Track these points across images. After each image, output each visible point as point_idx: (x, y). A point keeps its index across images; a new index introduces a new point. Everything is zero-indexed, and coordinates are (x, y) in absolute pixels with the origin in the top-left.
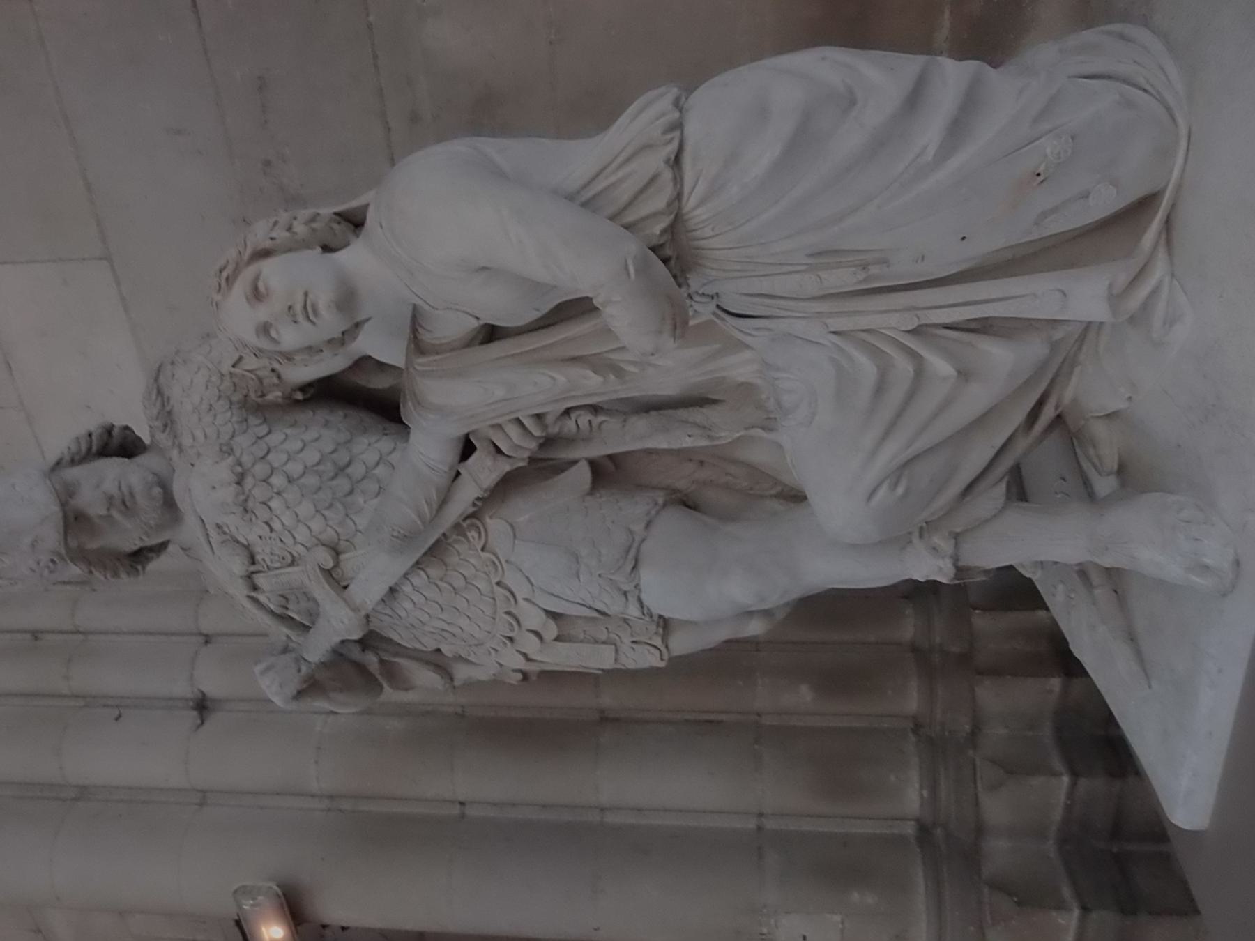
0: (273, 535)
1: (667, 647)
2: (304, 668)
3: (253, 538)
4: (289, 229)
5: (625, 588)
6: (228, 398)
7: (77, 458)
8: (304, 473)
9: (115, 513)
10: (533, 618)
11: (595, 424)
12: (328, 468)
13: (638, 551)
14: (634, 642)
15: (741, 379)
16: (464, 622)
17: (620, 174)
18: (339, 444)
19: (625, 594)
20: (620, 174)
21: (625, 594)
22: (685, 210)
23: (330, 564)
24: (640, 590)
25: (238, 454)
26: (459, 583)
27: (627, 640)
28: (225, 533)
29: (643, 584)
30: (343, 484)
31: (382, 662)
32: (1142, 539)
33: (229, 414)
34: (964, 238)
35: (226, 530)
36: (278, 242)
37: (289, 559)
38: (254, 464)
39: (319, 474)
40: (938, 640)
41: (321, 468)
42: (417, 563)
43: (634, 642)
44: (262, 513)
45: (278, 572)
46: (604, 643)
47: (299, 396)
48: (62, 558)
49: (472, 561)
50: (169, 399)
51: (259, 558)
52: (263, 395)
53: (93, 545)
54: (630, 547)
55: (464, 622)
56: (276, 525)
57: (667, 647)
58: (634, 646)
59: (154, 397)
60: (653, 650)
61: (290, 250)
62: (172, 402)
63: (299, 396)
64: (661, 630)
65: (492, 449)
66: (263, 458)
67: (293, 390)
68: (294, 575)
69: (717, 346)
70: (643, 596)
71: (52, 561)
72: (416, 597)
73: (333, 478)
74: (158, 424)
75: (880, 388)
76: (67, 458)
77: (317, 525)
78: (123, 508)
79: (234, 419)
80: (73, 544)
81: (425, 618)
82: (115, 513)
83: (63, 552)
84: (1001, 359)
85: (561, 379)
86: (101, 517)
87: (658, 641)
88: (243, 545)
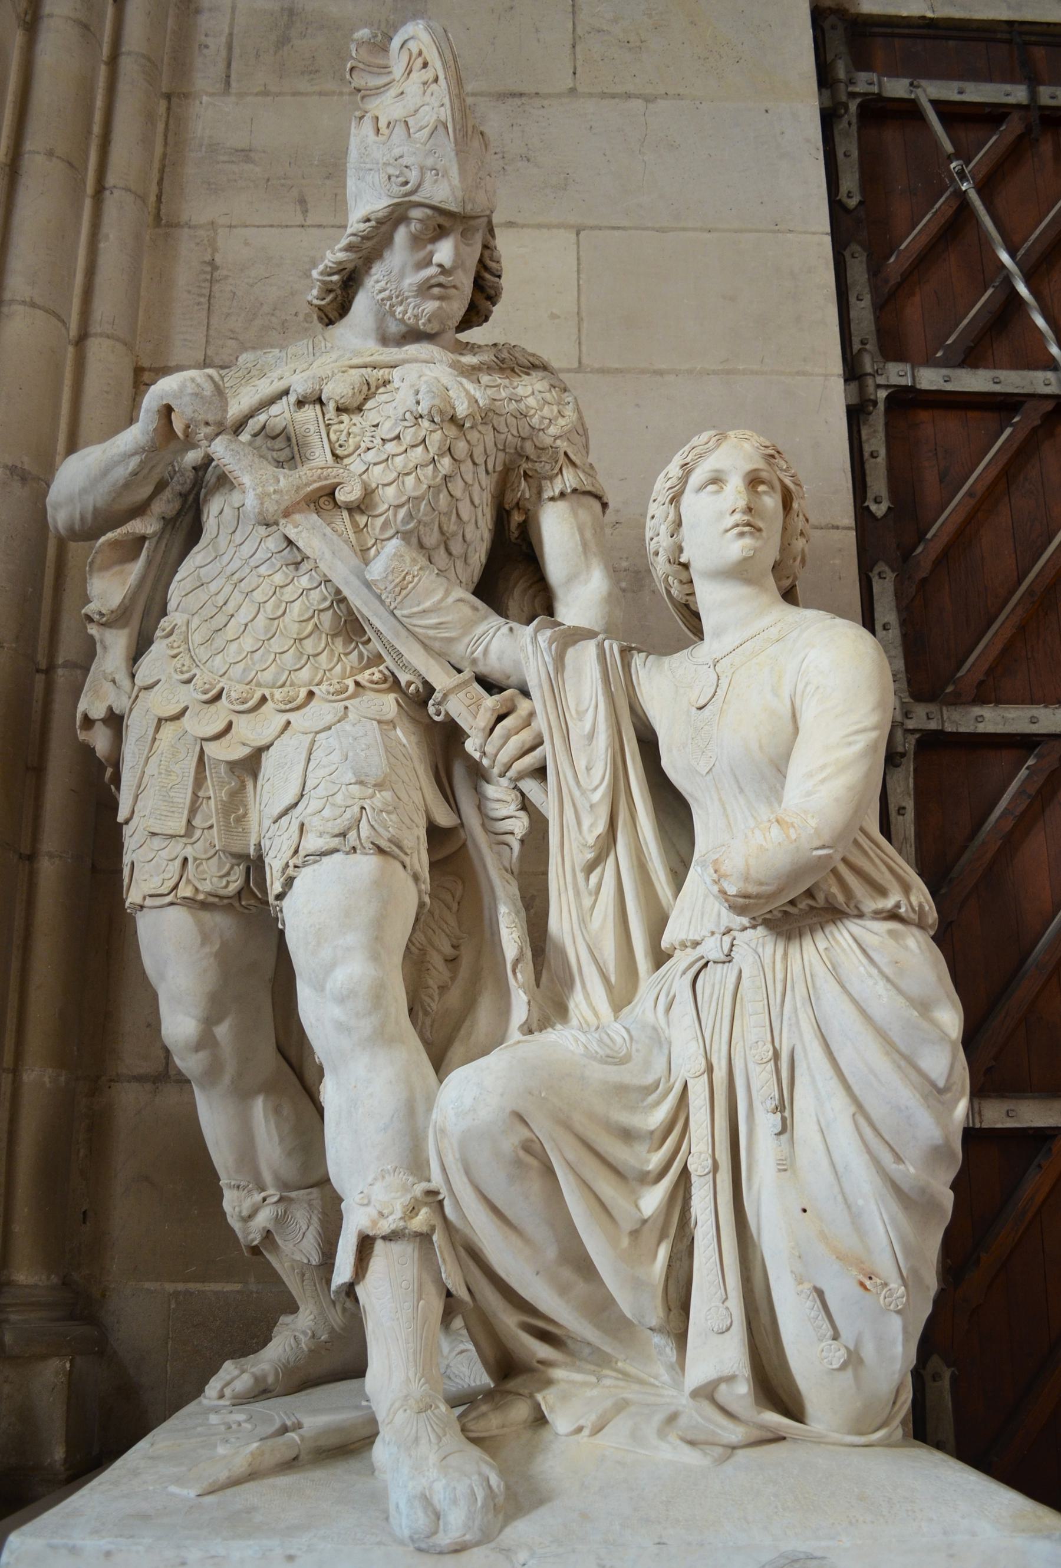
0: (378, 441)
1: (172, 904)
2: (205, 431)
3: (371, 415)
4: (802, 534)
5: (352, 835)
6: (530, 438)
7: (487, 253)
8: (451, 495)
9: (432, 270)
10: (251, 732)
11: (508, 838)
12: (452, 527)
13: (395, 857)
14: (186, 860)
15: (571, 1005)
16: (248, 643)
17: (877, 861)
18: (468, 545)
19: (343, 835)
20: (877, 861)
21: (343, 835)
22: (848, 923)
23: (341, 496)
24: (348, 853)
25: (480, 428)
26: (309, 646)
27: (189, 852)
28: (377, 388)
29: (357, 857)
30: (432, 538)
31: (143, 539)
32: (419, 1468)
33: (515, 433)
34: (805, 1211)
35: (381, 390)
36: (796, 519)
37: (339, 452)
38: (468, 442)
39: (448, 514)
40: (13, 1317)
41: (454, 517)
42: (343, 600)
43: (186, 860)
44: (408, 438)
45: (324, 436)
46: (189, 821)
47: (517, 518)
48: (406, 195)
49: (339, 667)
50: (528, 374)
51: (345, 417)
52: (526, 475)
53: (401, 235)
54: (400, 848)
55: (248, 643)
56: (391, 447)
57: (172, 904)
58: (178, 863)
59: (531, 359)
60: (171, 884)
61: (785, 529)
62: (524, 377)
63: (517, 518)
64: (201, 897)
65: (504, 710)
66: (471, 456)
67: (527, 512)
68: (321, 456)
69: (613, 979)
70: (336, 856)
71: (406, 183)
72: (289, 593)
73: (440, 527)
74: (505, 355)
75: (627, 1135)
76: (492, 243)
77: (390, 493)
78: (433, 281)
79: (510, 436)
80: (416, 213)
81: (258, 596)
82: (432, 270)
83: (414, 198)
84: (632, 1283)
85: (597, 796)
86: (431, 254)
87: (184, 891)
88: (363, 404)
